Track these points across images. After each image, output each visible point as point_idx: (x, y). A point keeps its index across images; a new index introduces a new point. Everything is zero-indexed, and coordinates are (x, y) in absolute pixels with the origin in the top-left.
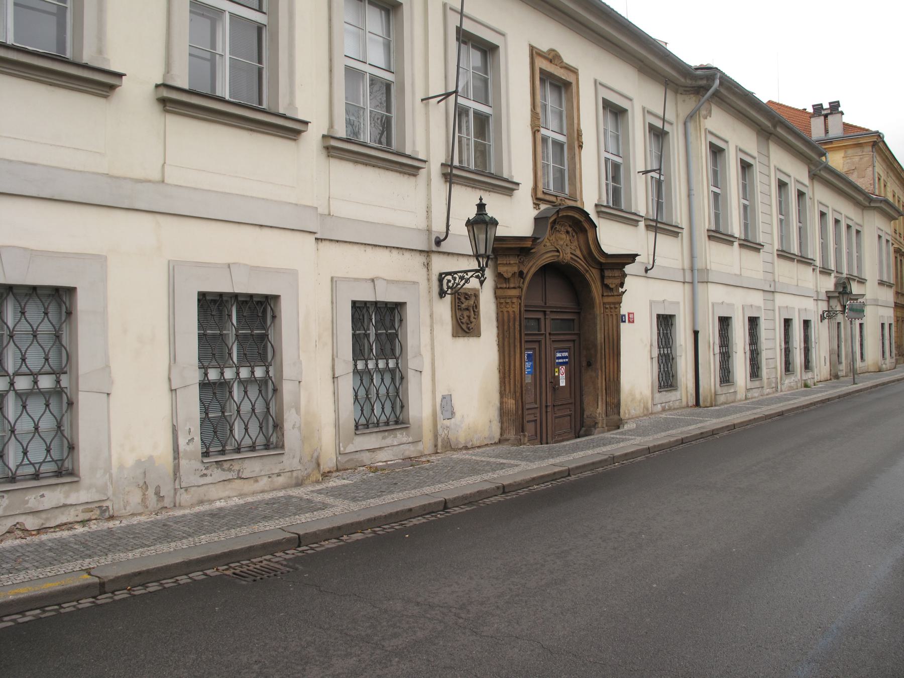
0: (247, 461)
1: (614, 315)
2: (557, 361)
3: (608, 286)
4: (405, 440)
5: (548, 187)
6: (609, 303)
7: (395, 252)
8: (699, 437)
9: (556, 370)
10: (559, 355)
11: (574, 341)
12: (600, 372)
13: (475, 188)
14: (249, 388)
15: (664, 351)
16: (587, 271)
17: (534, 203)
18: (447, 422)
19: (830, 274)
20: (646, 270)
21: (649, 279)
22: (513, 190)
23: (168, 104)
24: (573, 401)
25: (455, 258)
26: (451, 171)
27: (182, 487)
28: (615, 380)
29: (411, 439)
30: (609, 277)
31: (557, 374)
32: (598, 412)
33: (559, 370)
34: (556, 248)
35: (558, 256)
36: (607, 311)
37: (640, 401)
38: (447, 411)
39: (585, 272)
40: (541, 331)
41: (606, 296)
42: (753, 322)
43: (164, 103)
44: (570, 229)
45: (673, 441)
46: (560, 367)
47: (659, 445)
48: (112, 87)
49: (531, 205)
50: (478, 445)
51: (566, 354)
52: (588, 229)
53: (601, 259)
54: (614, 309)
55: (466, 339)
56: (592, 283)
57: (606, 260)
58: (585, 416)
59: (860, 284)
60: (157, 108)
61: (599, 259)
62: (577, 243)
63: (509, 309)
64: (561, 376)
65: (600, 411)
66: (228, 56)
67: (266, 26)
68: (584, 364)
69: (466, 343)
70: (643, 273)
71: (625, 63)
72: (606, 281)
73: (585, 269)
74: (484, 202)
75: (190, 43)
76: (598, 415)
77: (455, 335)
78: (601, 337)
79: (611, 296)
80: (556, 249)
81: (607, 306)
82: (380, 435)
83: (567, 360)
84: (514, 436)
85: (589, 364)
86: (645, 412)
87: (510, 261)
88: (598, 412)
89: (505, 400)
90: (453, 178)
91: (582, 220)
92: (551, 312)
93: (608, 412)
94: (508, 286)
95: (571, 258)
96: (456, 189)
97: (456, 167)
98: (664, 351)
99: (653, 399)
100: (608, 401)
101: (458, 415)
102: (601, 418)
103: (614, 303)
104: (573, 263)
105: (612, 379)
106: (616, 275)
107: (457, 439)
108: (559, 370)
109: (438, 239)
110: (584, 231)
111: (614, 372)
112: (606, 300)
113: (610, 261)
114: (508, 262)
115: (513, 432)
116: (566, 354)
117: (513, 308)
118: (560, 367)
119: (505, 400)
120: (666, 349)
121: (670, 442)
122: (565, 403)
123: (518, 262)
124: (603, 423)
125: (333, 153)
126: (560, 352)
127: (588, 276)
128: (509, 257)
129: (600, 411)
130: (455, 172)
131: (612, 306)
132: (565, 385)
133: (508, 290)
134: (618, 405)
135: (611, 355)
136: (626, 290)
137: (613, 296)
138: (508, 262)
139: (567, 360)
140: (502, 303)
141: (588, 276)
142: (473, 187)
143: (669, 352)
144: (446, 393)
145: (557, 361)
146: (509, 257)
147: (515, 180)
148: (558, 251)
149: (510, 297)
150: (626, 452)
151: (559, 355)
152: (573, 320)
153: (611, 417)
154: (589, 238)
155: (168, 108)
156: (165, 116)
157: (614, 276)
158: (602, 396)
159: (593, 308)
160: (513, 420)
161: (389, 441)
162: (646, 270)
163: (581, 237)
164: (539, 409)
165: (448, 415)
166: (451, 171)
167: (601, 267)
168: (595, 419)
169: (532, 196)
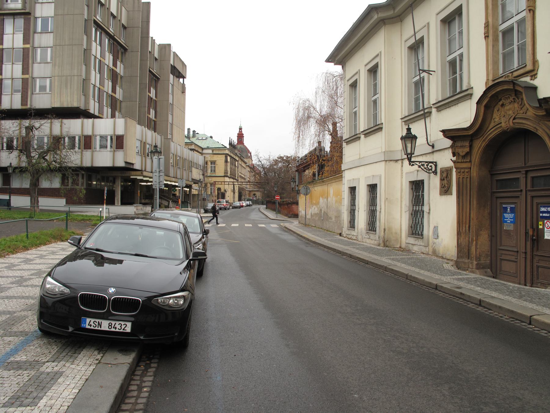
0: (371, 234)
2: (541, 215)
4: (421, 244)
7: (424, 156)
9: (540, 223)
10: (543, 209)
13: (450, 107)
14: (11, 196)
15: (416, 208)
18: (435, 240)
19: (359, 138)
25: (443, 151)
27: (539, 268)
29: (423, 244)
31: (541, 227)
33: (543, 223)
38: (435, 234)
42: (373, 188)
45: (426, 281)
46: (545, 221)
47: (414, 277)
48: (382, 128)
50: (448, 258)
55: (446, 196)
69: (445, 198)
71: (373, 37)
74: (410, 127)
77: (441, 194)
82: (415, 239)
98: (416, 208)
101: (440, 237)
107: (439, 250)
108: (543, 223)
114: (462, 145)
118: (545, 221)
120: (417, 207)
121: (424, 280)
125: (440, 109)
126: (544, 207)
138: (462, 145)
142: (449, 107)
143: (375, 209)
144: (436, 225)
145: (541, 215)
151: (543, 209)
157: (463, 146)
161: (416, 242)
165: (436, 237)
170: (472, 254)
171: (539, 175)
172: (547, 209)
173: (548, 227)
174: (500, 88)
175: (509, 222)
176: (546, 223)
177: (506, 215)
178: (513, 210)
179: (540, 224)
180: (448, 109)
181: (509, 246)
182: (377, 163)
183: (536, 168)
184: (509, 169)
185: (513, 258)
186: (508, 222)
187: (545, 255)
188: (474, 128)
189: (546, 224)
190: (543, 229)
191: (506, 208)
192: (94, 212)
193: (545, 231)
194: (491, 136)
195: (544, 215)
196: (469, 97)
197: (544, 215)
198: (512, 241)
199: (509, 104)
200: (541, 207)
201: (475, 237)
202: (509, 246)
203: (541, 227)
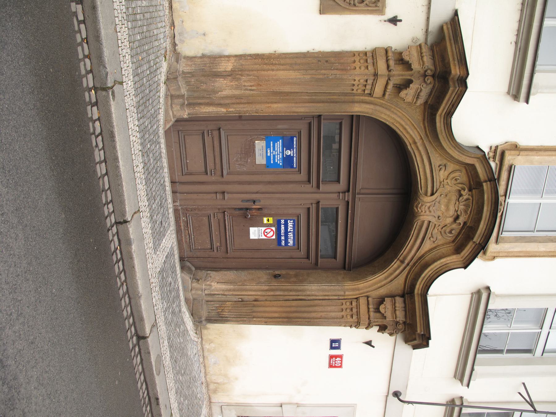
1: (343, 313)
2: (283, 222)
3: (383, 303)
5: (479, 350)
6: (358, 307)
8: (151, 395)
11: (308, 258)
12: (266, 288)
16: (402, 262)
17: (497, 147)
20: (397, 394)
21: (384, 399)
22: (461, 380)
23: (477, 296)
24: (226, 177)
26: (457, 406)
28: (254, 314)
30: (395, 303)
32: (213, 284)
33: (271, 225)
34: (436, 192)
35: (426, 194)
36: (348, 304)
37: (226, 376)
39: (401, 258)
40: (322, 184)
41: (368, 301)
43: (478, 293)
44: (461, 220)
46: (274, 229)
49: (494, 143)
51: (291, 242)
52: (462, 254)
53: (420, 284)
54: (351, 306)
56: (386, 274)
57: (418, 294)
58: (209, 272)
59: (490, 147)
60: (474, 289)
61: (418, 283)
62: (440, 243)
63: (357, 63)
64: (263, 229)
65: (213, 288)
66: (510, 331)
67: (534, 356)
68: (277, 272)
70: (393, 390)
72: (388, 301)
73: (405, 258)
75: (543, 203)
76: (208, 283)
78: (312, 290)
79: (368, 308)
80: (434, 192)
81: (354, 304)
83: (283, 243)
84: (181, 70)
85: (276, 276)
86: (212, 387)
87: (426, 56)
88: (213, 284)
89: (233, 60)
90: (450, 408)
91: (475, 240)
92: (348, 202)
93: (212, 303)
94: (390, 58)
95: (423, 222)
96: (444, 408)
97: (461, 410)
99: (229, 405)
100: (227, 303)
102: (204, 287)
103: (359, 318)
104: (416, 226)
105: (255, 309)
106: (398, 313)
108: (271, 225)
109: (399, 394)
110: (458, 250)
111: (265, 312)
112: (363, 301)
113: (417, 299)
115: (187, 69)
116: (291, 242)
117: (360, 68)
118: (274, 229)
119: (233, 60)
122: (233, 259)
123: (398, 319)
124: (197, 289)
126: (294, 225)
127: (395, 266)
128: (404, 310)
129: (213, 288)
130: (457, 410)
131: (355, 310)
132: (251, 238)
133: (384, 60)
134: (220, 319)
135: (288, 309)
136: (373, 347)
137: (368, 311)
139: (283, 243)
140: (352, 304)
141: (395, 266)
142: (518, 30)
145: (283, 222)
146: (404, 310)
147: (532, 98)
148: (432, 194)
149: (374, 64)
150: (117, 138)
151: (290, 224)
152: (335, 257)
153: (205, 307)
154: (448, 258)
155: (474, 296)
156: (468, 294)
157: (395, 310)
158: (234, 290)
159: (351, 281)
160: (204, 69)
162: (397, 394)
163: (450, 248)
164: (220, 179)
166: (457, 406)
167: (407, 294)
168: (203, 279)
169: (506, 143)
170: (201, 108)
171: (340, 222)
172: (290, 232)
173: (266, 234)
174: (486, 216)
175: (269, 154)
176: (272, 230)
177: (279, 144)
178: (288, 160)
179: (269, 218)
180: (514, 39)
181: (229, 154)
182: (425, 9)
183: (349, 221)
184: (356, 158)
185: (210, 165)
186: (269, 151)
187: (227, 232)
188: (444, 134)
189: (270, 230)
190: (263, 225)
191: (290, 147)
192: (368, 10)
193: (261, 228)
194: (418, 159)
195: (283, 227)
196: (513, 91)
197: (283, 227)
198: (237, 161)
199: (457, 209)
200: (294, 220)
201: (233, 110)
202: (229, 154)
203: (265, 220)
